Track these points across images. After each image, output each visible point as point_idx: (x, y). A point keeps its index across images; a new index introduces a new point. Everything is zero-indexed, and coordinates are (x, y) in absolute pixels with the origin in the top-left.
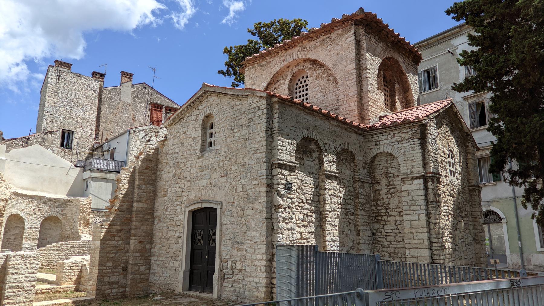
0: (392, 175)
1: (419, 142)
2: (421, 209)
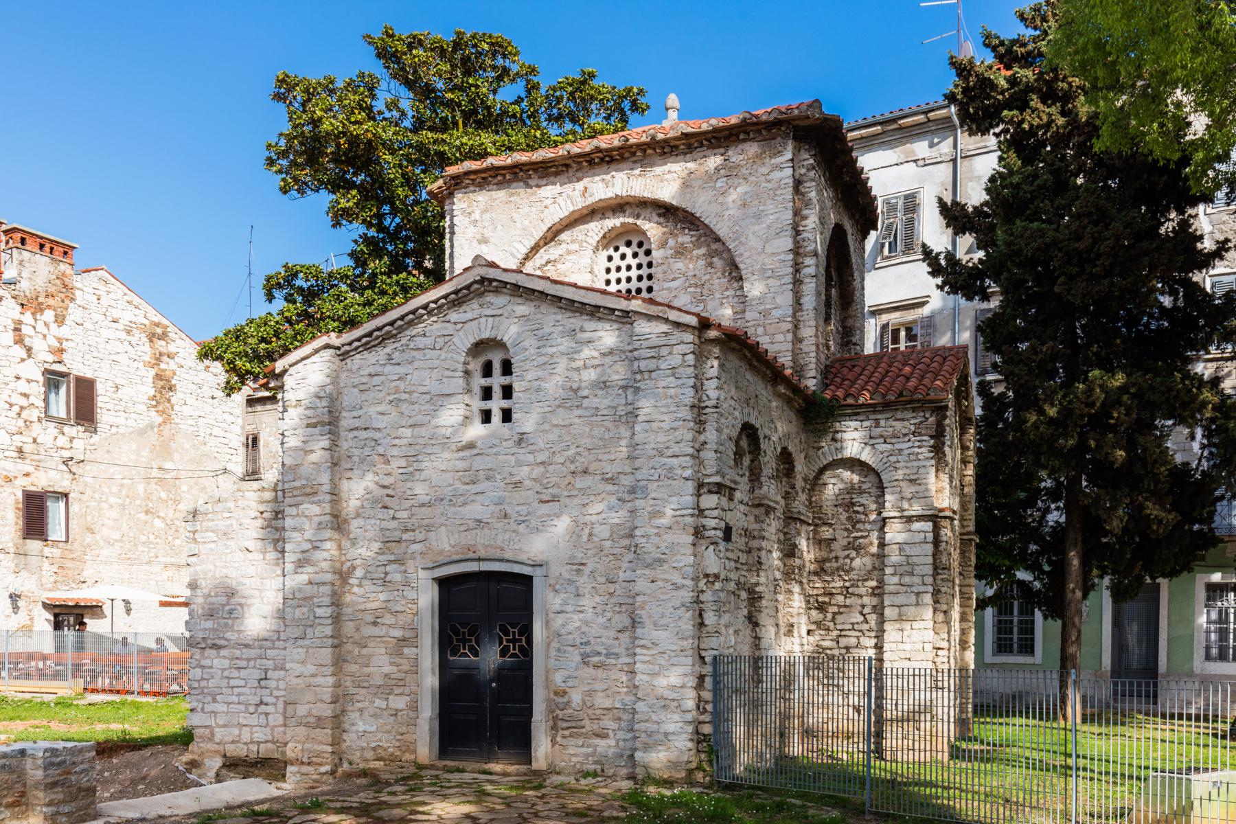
0: (860, 509)
1: (932, 442)
2: (924, 584)
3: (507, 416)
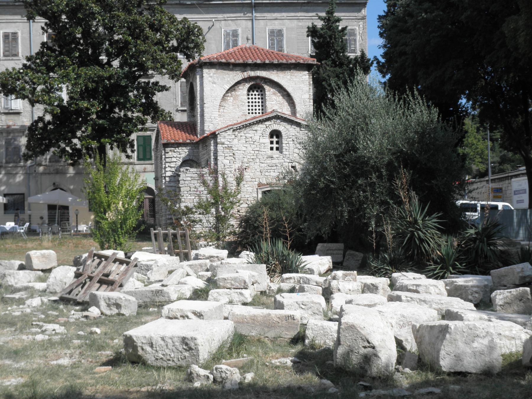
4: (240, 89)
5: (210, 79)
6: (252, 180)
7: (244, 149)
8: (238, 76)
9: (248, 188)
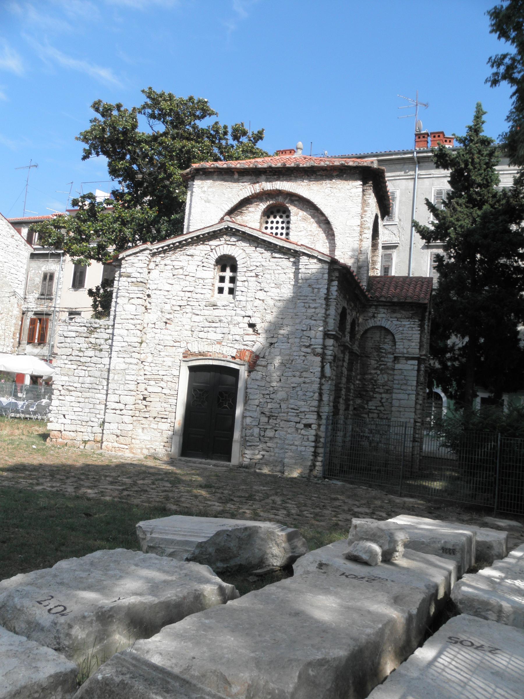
0: (384, 351)
3: (231, 291)
4: (249, 212)
5: (202, 195)
6: (175, 344)
7: (168, 287)
8: (245, 189)
9: (166, 359)
